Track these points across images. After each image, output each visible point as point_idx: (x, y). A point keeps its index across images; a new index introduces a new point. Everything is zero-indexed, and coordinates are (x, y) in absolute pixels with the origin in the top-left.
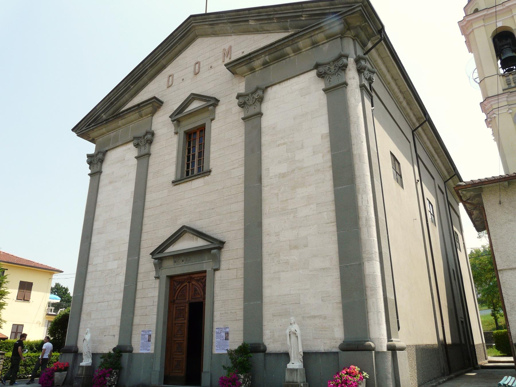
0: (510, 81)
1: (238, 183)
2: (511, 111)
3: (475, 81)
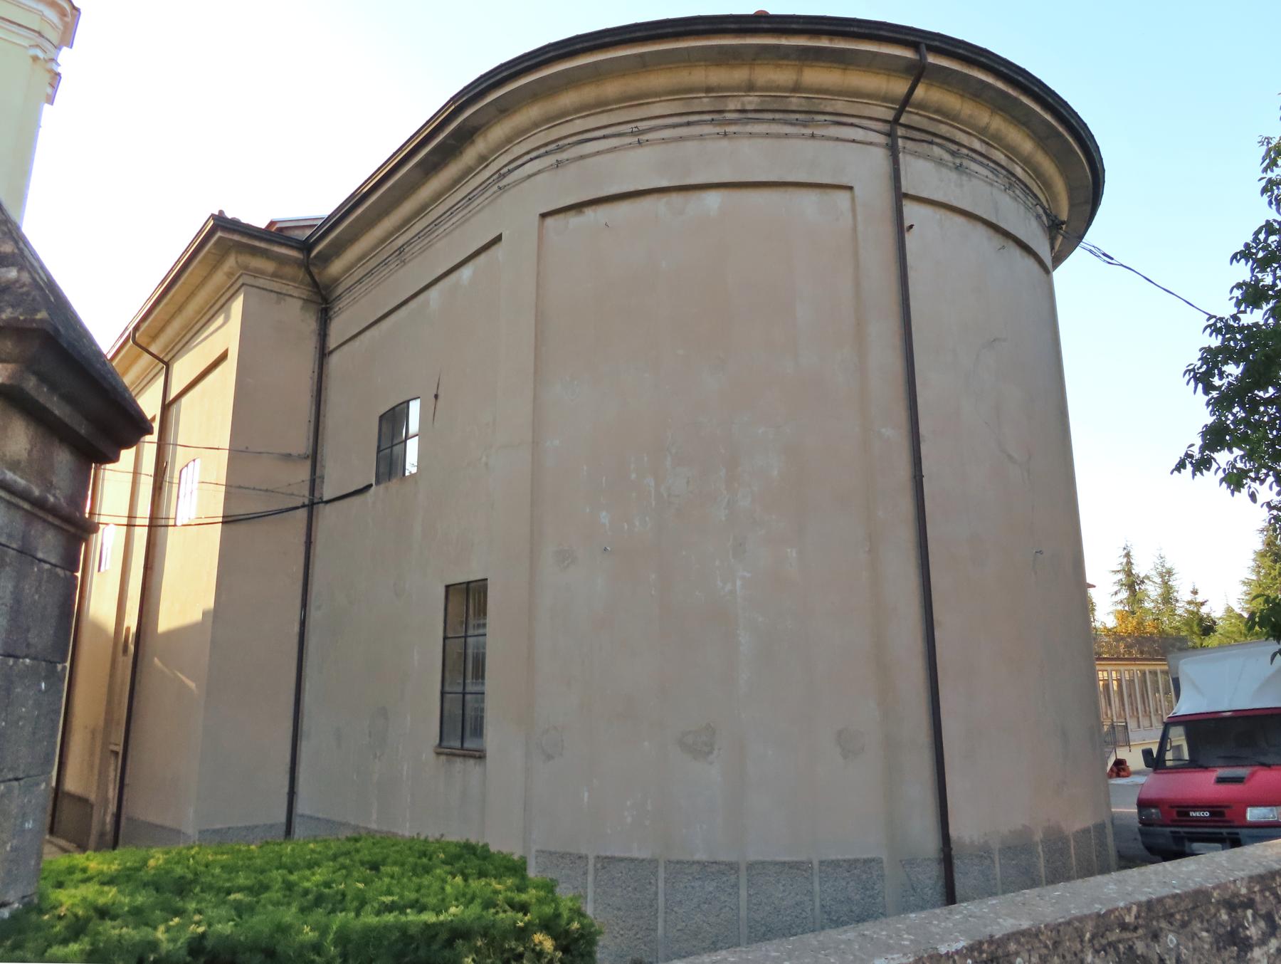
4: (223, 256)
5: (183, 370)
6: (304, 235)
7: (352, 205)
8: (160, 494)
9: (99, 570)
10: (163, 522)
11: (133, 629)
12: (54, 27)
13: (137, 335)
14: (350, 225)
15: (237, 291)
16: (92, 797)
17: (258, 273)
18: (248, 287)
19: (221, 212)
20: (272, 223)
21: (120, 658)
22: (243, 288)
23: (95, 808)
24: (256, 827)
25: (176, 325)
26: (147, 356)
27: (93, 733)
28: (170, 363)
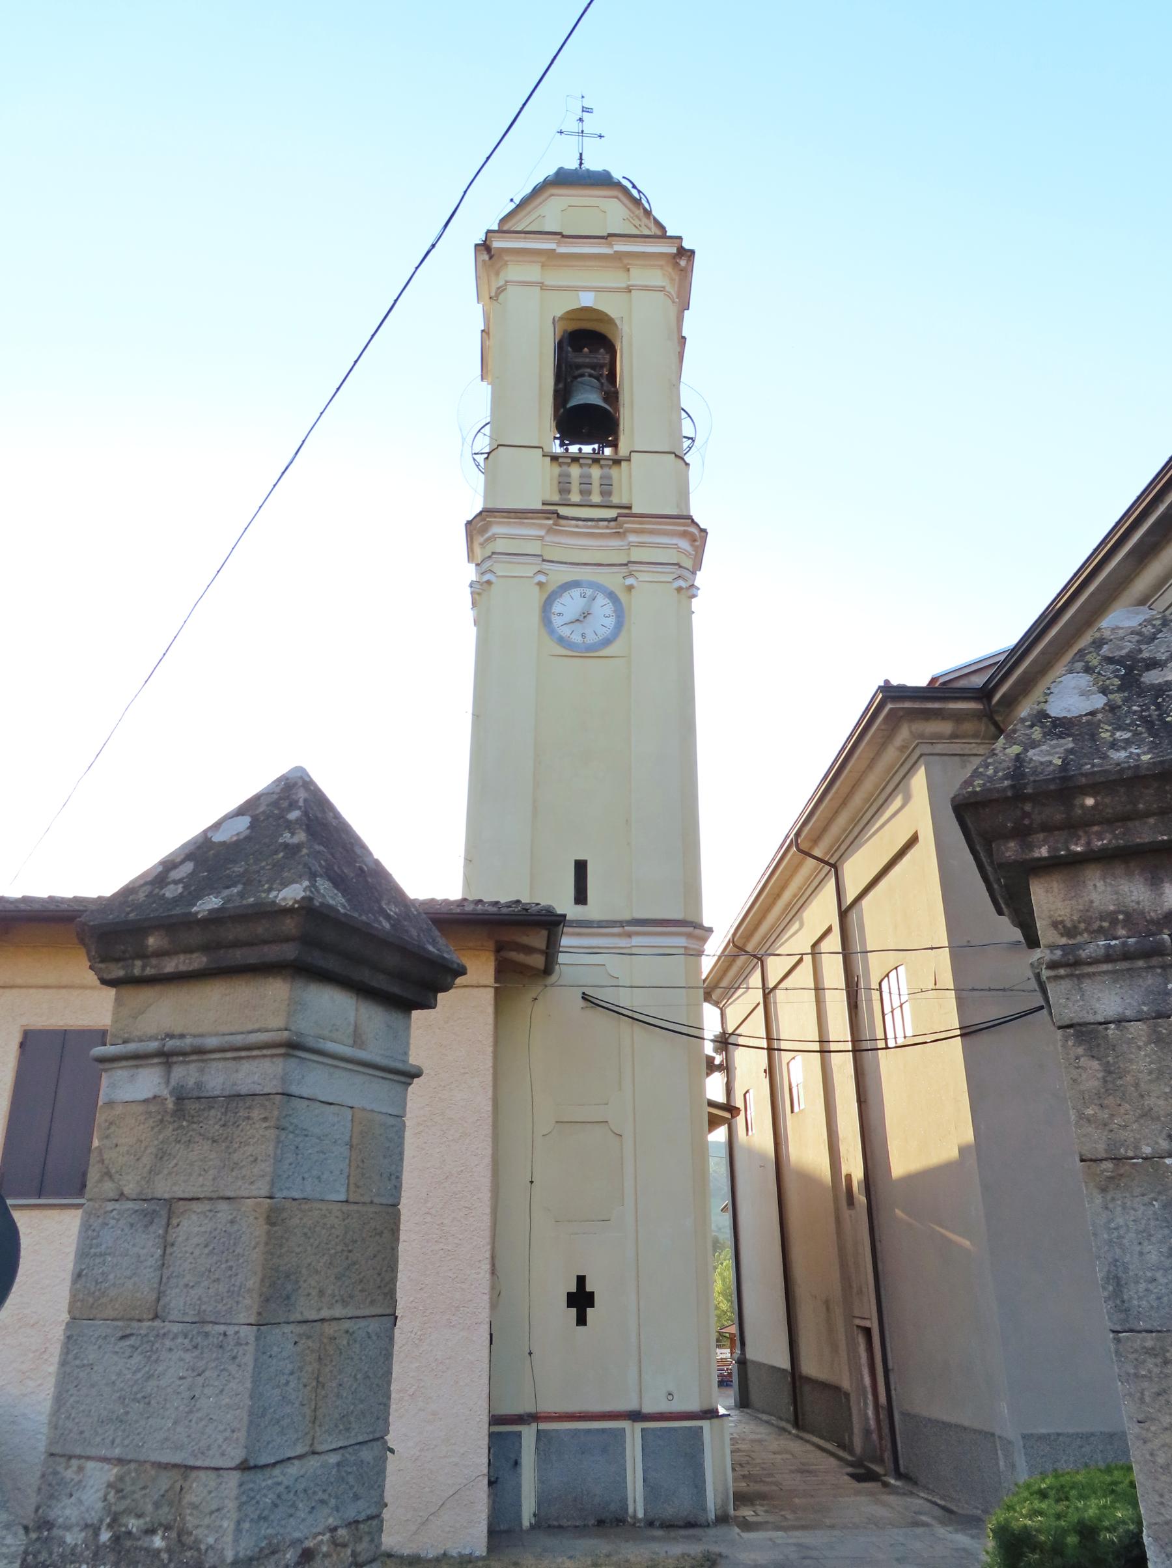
0: (570, 483)
1: (104, 1263)
2: (542, 578)
3: (474, 459)
4: (893, 730)
5: (856, 872)
6: (979, 681)
7: (1044, 626)
8: (856, 1014)
9: (792, 1111)
10: (869, 1045)
11: (858, 1174)
12: (686, 553)
13: (799, 842)
14: (1042, 653)
15: (916, 763)
16: (846, 1384)
17: (937, 737)
18: (927, 757)
19: (887, 682)
20: (933, 680)
21: (846, 1212)
22: (922, 759)
23: (851, 1395)
24: (1092, 1434)
25: (842, 820)
26: (811, 862)
27: (827, 1304)
28: (837, 864)
